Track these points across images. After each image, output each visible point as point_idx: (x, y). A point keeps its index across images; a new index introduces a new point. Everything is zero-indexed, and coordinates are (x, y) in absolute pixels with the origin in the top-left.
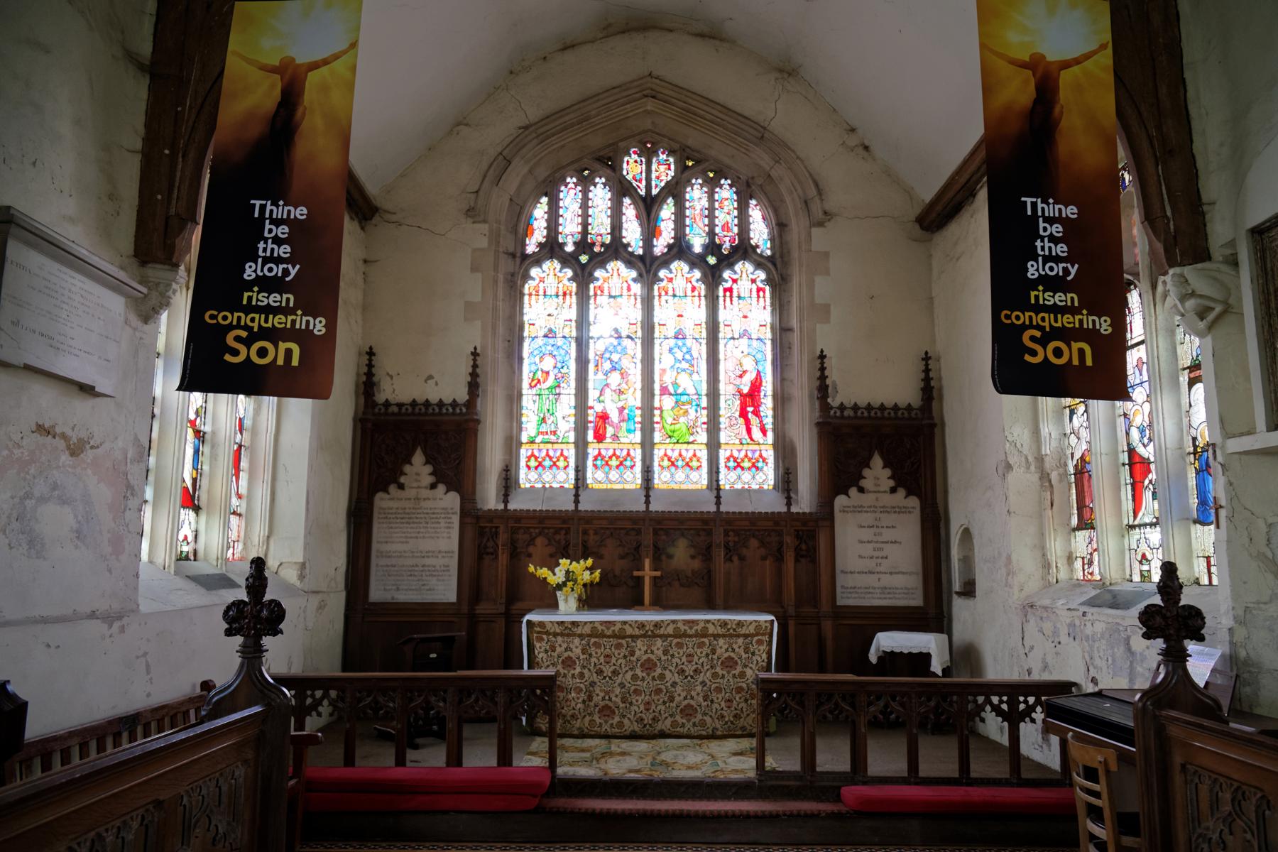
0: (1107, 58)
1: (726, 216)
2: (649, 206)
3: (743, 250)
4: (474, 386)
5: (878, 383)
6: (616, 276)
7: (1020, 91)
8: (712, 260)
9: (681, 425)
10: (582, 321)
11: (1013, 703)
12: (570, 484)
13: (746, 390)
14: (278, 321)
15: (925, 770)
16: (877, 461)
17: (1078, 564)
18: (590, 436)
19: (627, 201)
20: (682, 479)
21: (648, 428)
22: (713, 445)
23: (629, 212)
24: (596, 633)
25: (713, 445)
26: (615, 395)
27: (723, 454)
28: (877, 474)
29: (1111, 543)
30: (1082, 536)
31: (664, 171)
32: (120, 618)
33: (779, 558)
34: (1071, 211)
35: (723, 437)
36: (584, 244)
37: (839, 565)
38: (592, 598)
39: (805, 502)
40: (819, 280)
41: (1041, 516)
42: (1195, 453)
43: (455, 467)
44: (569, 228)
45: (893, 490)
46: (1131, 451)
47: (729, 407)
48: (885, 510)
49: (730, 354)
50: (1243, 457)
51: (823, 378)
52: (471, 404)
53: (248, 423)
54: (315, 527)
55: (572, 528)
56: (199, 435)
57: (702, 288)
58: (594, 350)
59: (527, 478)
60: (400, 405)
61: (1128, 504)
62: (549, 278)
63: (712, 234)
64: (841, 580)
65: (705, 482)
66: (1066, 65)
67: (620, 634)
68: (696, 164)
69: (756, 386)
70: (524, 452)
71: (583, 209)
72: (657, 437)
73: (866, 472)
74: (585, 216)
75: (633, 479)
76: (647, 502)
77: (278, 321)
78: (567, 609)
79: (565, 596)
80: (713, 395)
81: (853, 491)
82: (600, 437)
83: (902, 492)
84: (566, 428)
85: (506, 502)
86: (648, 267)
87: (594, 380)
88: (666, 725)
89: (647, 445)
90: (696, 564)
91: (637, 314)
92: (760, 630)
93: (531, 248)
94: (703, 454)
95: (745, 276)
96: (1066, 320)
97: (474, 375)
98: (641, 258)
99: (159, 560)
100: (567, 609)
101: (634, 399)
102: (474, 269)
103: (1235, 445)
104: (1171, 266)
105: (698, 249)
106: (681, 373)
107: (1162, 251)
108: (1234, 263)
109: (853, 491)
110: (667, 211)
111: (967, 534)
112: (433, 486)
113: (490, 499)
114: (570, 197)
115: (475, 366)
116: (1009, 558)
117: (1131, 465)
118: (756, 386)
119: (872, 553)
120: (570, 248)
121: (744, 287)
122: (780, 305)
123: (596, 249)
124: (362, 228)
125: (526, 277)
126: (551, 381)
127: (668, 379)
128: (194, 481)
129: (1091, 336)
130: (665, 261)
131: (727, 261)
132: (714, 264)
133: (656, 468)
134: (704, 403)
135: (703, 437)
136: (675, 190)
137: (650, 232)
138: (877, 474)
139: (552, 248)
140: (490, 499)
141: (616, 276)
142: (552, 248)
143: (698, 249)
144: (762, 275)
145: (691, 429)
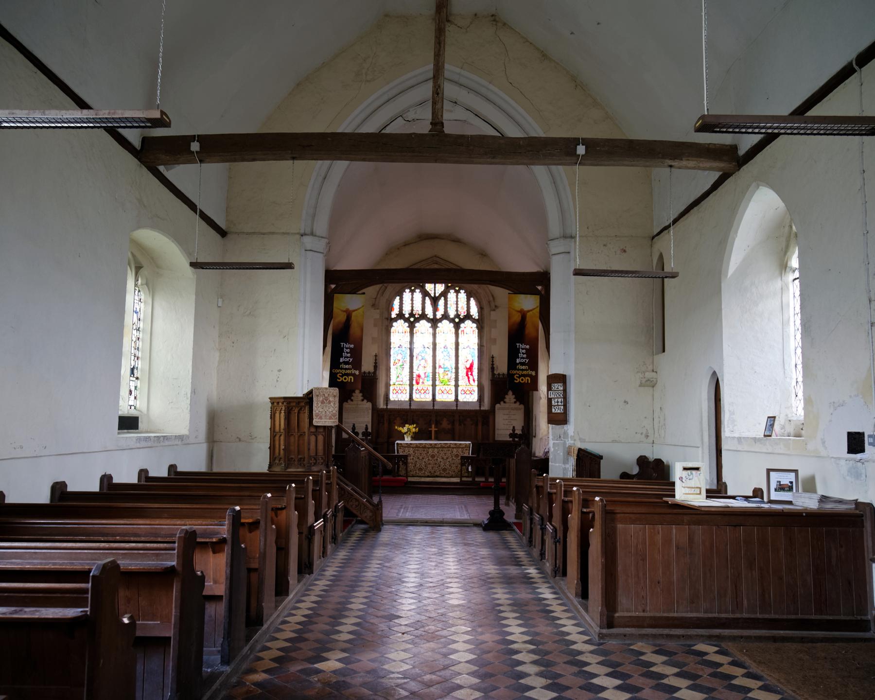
0: (538, 310)
2: (435, 301)
3: (468, 316)
4: (376, 367)
7: (517, 318)
9: (446, 376)
10: (411, 342)
12: (407, 399)
14: (348, 371)
16: (510, 393)
18: (414, 382)
19: (427, 298)
20: (445, 396)
21: (434, 379)
22: (457, 386)
24: (417, 446)
25: (457, 386)
27: (460, 389)
28: (510, 397)
31: (440, 288)
33: (477, 425)
34: (528, 347)
35: (460, 383)
36: (412, 314)
37: (497, 427)
38: (415, 437)
39: (486, 406)
40: (493, 330)
44: (407, 311)
47: (462, 372)
48: (512, 409)
51: (493, 365)
52: (375, 373)
59: (393, 397)
63: (457, 310)
64: (497, 432)
66: (529, 311)
67: (424, 447)
69: (472, 366)
70: (391, 388)
71: (411, 300)
72: (437, 383)
77: (348, 371)
78: (408, 440)
79: (406, 436)
80: (457, 368)
81: (502, 403)
82: (418, 383)
83: (518, 403)
86: (434, 322)
88: (438, 474)
89: (434, 386)
90: (450, 426)
91: (431, 340)
92: (467, 446)
93: (393, 315)
94: (453, 389)
96: (525, 372)
97: (376, 363)
98: (432, 320)
100: (408, 440)
101: (430, 370)
102: (375, 325)
106: (446, 360)
109: (502, 403)
110: (441, 302)
113: (381, 405)
114: (407, 295)
118: (472, 366)
120: (407, 316)
125: (392, 326)
126: (401, 363)
129: (530, 376)
130: (440, 320)
131: (462, 321)
135: (453, 383)
136: (444, 294)
137: (435, 309)
138: (510, 397)
139: (401, 316)
140: (381, 405)
141: (423, 327)
142: (401, 316)
145: (449, 380)
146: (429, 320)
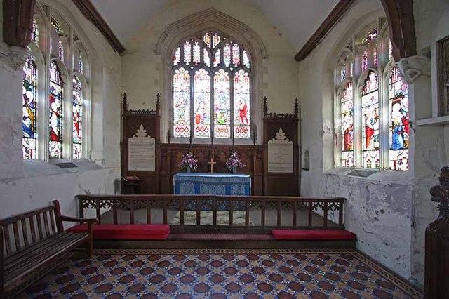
1: (236, 56)
2: (212, 52)
3: (241, 66)
5: (281, 107)
6: (202, 73)
8: (231, 69)
9: (222, 116)
11: (326, 204)
12: (189, 136)
13: (242, 109)
15: (299, 223)
16: (281, 130)
17: (344, 162)
18: (195, 122)
19: (205, 50)
20: (222, 134)
22: (232, 125)
23: (206, 53)
25: (232, 125)
26: (202, 109)
27: (235, 128)
28: (281, 134)
29: (358, 156)
30: (346, 153)
32: (13, 179)
35: (235, 123)
36: (192, 63)
39: (259, 142)
41: (333, 147)
42: (393, 127)
43: (153, 130)
45: (285, 139)
46: (367, 127)
47: (237, 114)
49: (237, 99)
50: (425, 127)
52: (157, 111)
53: (81, 114)
54: (107, 147)
55: (191, 147)
56: (58, 116)
57: (228, 78)
58: (196, 96)
59: (176, 134)
60: (135, 111)
61: (364, 144)
62: (181, 73)
63: (232, 61)
65: (229, 136)
68: (226, 39)
70: (175, 127)
71: (191, 52)
73: (277, 134)
74: (192, 54)
75: (208, 135)
76: (212, 142)
84: (188, 119)
85: (169, 141)
86: (212, 71)
87: (196, 106)
89: (212, 125)
94: (229, 128)
95: (242, 75)
99: (43, 158)
101: (208, 112)
103: (420, 122)
104: (402, 57)
105: (227, 65)
106: (222, 103)
107: (399, 53)
108: (429, 55)
110: (218, 53)
111: (307, 152)
112: (147, 136)
114: (187, 48)
115: (158, 100)
116: (322, 160)
117: (366, 131)
119: (278, 158)
120: (187, 64)
121: (241, 78)
122: (252, 83)
123: (196, 64)
124: (120, 55)
125: (174, 73)
127: (218, 106)
128: (59, 132)
130: (217, 69)
131: (236, 70)
132: (232, 71)
133: (215, 132)
134: (229, 113)
135: (229, 123)
137: (212, 60)
138: (281, 134)
140: (164, 141)
142: (182, 64)
143: (227, 65)
144: (247, 74)
146: (206, 69)
